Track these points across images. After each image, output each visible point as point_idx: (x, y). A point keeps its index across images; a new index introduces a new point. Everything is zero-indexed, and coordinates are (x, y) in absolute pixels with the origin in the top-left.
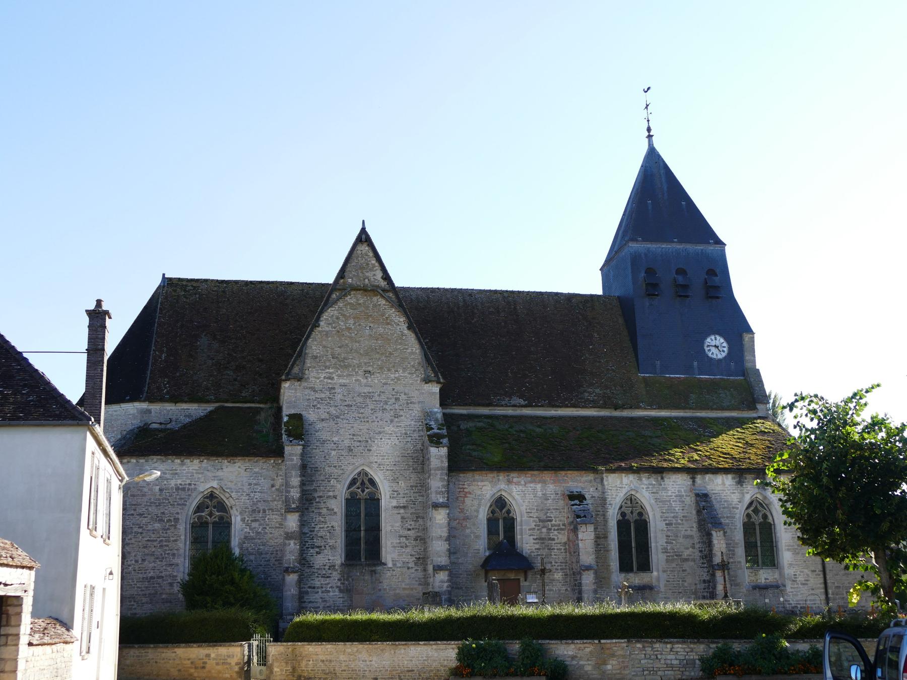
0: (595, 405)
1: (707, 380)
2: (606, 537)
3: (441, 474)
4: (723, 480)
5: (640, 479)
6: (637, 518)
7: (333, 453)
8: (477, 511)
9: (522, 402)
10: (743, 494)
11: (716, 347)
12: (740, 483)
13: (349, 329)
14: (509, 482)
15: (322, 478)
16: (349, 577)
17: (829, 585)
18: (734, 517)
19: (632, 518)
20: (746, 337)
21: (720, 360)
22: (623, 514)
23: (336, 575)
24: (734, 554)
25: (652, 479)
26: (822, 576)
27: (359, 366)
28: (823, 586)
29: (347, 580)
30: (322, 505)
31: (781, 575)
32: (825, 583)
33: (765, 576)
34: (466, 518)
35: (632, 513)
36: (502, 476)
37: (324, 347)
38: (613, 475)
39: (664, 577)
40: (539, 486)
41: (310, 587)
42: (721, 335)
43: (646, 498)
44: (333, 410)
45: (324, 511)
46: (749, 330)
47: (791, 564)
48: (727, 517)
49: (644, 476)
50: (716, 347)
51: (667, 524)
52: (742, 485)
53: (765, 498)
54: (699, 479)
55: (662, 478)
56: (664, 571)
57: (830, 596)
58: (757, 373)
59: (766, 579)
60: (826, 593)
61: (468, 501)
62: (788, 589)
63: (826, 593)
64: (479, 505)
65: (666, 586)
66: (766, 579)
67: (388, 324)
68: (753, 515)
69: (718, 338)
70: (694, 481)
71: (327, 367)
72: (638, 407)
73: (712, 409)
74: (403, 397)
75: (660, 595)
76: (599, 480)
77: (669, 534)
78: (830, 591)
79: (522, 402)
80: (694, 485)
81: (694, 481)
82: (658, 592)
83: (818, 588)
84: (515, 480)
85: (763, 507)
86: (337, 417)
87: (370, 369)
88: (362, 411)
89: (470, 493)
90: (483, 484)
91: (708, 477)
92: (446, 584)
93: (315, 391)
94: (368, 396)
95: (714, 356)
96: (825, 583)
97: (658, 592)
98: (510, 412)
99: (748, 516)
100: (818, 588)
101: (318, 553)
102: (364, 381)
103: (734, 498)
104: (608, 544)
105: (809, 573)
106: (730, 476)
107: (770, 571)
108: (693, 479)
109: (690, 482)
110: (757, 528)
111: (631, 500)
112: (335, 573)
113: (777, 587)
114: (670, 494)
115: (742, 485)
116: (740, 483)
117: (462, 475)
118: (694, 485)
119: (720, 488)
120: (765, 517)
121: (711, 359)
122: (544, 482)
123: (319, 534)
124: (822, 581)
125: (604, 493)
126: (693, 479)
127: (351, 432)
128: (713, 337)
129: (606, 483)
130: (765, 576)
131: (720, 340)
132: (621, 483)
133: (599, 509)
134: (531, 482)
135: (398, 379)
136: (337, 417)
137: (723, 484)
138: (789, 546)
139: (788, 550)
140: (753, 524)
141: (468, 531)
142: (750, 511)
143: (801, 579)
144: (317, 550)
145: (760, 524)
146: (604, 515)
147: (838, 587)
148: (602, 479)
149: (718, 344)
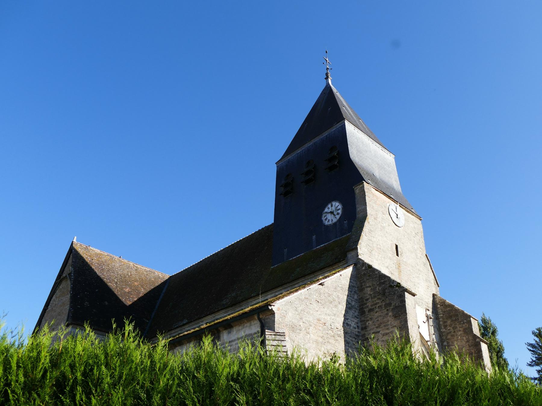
11: (332, 213)
21: (335, 224)
50: (332, 213)
69: (334, 203)
128: (330, 206)
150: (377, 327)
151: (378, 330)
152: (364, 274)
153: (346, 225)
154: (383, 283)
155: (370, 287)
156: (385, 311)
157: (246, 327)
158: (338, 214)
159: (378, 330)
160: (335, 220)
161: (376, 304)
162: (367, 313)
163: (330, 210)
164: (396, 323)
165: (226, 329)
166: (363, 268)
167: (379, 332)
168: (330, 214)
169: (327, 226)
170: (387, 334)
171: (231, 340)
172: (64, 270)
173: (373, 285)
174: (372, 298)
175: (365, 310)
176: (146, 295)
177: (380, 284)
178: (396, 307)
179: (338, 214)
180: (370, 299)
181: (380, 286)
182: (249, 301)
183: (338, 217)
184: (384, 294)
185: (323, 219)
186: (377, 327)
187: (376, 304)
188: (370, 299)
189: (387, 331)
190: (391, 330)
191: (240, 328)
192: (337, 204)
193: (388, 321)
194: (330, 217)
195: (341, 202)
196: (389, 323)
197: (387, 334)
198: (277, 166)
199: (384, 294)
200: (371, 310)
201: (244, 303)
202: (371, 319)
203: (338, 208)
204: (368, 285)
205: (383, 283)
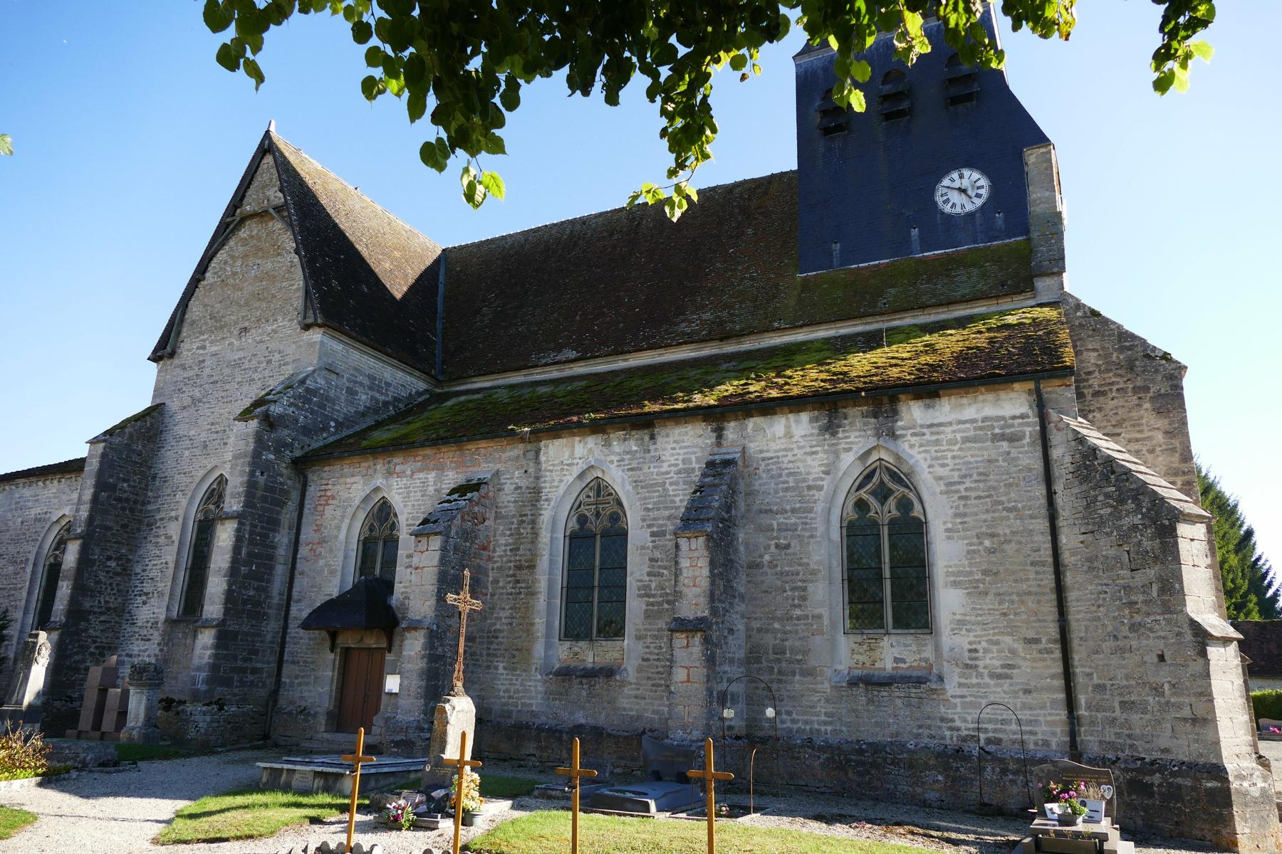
0: (690, 340)
1: (936, 258)
2: (532, 567)
3: (243, 465)
4: (788, 427)
5: (608, 444)
6: (607, 524)
7: (187, 453)
8: (338, 528)
9: (573, 354)
10: (836, 454)
11: (963, 191)
12: (831, 429)
13: (234, 274)
14: (390, 473)
15: (169, 491)
16: (170, 640)
17: (1080, 680)
18: (810, 510)
19: (595, 526)
20: (1032, 156)
21: (971, 215)
22: (582, 520)
23: (156, 637)
24: (804, 598)
25: (632, 442)
26: (1058, 654)
27: (236, 323)
28: (1060, 683)
29: (167, 644)
30: (161, 532)
31: (937, 648)
32: (1068, 675)
33: (894, 651)
34: (322, 541)
35: (598, 515)
36: (380, 466)
37: (205, 306)
38: (558, 442)
39: (639, 647)
40: (431, 476)
41: (127, 655)
42: (971, 165)
43: (617, 479)
44: (197, 393)
45: (162, 540)
46: (1040, 139)
47: (960, 622)
48: (794, 511)
49: (616, 437)
50: (963, 191)
51: (653, 534)
52: (834, 434)
53: (898, 457)
54: (732, 430)
55: (652, 437)
56: (639, 638)
57: (1082, 712)
58: (1055, 222)
59: (896, 660)
60: (1071, 704)
61: (329, 511)
62: (952, 687)
63: (1071, 704)
64: (343, 517)
65: (640, 670)
66: (896, 660)
67: (278, 254)
68: (873, 502)
69: (966, 172)
70: (720, 437)
71: (202, 333)
72: (769, 329)
73: (923, 307)
74: (277, 356)
75: (626, 691)
76: (531, 455)
77: (657, 554)
78: (1082, 699)
79: (573, 354)
80: (719, 444)
81: (720, 437)
82: (623, 684)
83: (1049, 689)
84: (398, 469)
85: (900, 481)
86: (200, 401)
87: (247, 324)
88: (227, 387)
89: (333, 498)
90: (353, 480)
91: (751, 423)
92: (208, 652)
93: (185, 369)
94: (237, 365)
95: (958, 210)
96: (1068, 675)
97: (623, 684)
98: (554, 373)
99: (861, 505)
100: (1049, 689)
101: (144, 603)
102: (236, 343)
103: (814, 465)
104: (535, 581)
105: (1019, 647)
106: (805, 417)
107: (909, 640)
108: (719, 433)
109: (711, 439)
110: (885, 531)
111: (600, 489)
112: (156, 634)
113: (919, 682)
114: (665, 468)
115: (834, 434)
116: (831, 429)
117: (326, 469)
118: (719, 444)
119: (778, 445)
120: (905, 505)
121: (950, 216)
122: (441, 469)
123: (151, 575)
124: (1058, 668)
125: (538, 478)
126: (719, 433)
127: (210, 420)
128: (955, 175)
129: (543, 458)
130: (896, 652)
131: (953, 180)
132: (572, 456)
133: (527, 511)
134: (420, 471)
135: (275, 331)
136: (200, 401)
137: (788, 435)
138: (959, 573)
139: (955, 584)
140: (875, 524)
141: (322, 562)
142: (863, 493)
143: (991, 661)
144: (144, 598)
145: (892, 523)
146: (533, 522)
147: (1100, 688)
148: (538, 452)
149: (965, 183)
150: (1114, 426)
151: (1117, 430)
152: (1081, 325)
153: (1000, 222)
154: (1129, 348)
155: (1095, 350)
156: (1134, 400)
157: (984, 401)
158: (978, 196)
159: (1117, 430)
160: (970, 207)
161: (1112, 384)
162: (1089, 398)
163: (957, 185)
164: (1162, 423)
165: (917, 397)
166: (1079, 314)
167: (1119, 435)
168: (956, 193)
169: (950, 217)
170: (1137, 440)
171: (935, 421)
172: (243, 196)
173: (1103, 348)
174: (1100, 372)
175: (1085, 391)
176: (418, 280)
177: (1122, 349)
178: (1159, 396)
179: (978, 196)
180: (1097, 374)
181: (1121, 353)
182: (766, 335)
183: (979, 202)
184: (1132, 369)
185: (939, 200)
186: (1114, 426)
187: (1112, 384)
188: (1097, 374)
189: (1139, 436)
190: (1147, 434)
191: (965, 401)
192: (976, 175)
193: (1141, 418)
194: (955, 197)
195: (985, 172)
196: (1144, 421)
197: (1137, 440)
198: (797, 66)
199: (1131, 368)
200: (1097, 394)
201: (752, 337)
202: (1100, 409)
203: (979, 184)
204: (1090, 347)
205: (1129, 348)
